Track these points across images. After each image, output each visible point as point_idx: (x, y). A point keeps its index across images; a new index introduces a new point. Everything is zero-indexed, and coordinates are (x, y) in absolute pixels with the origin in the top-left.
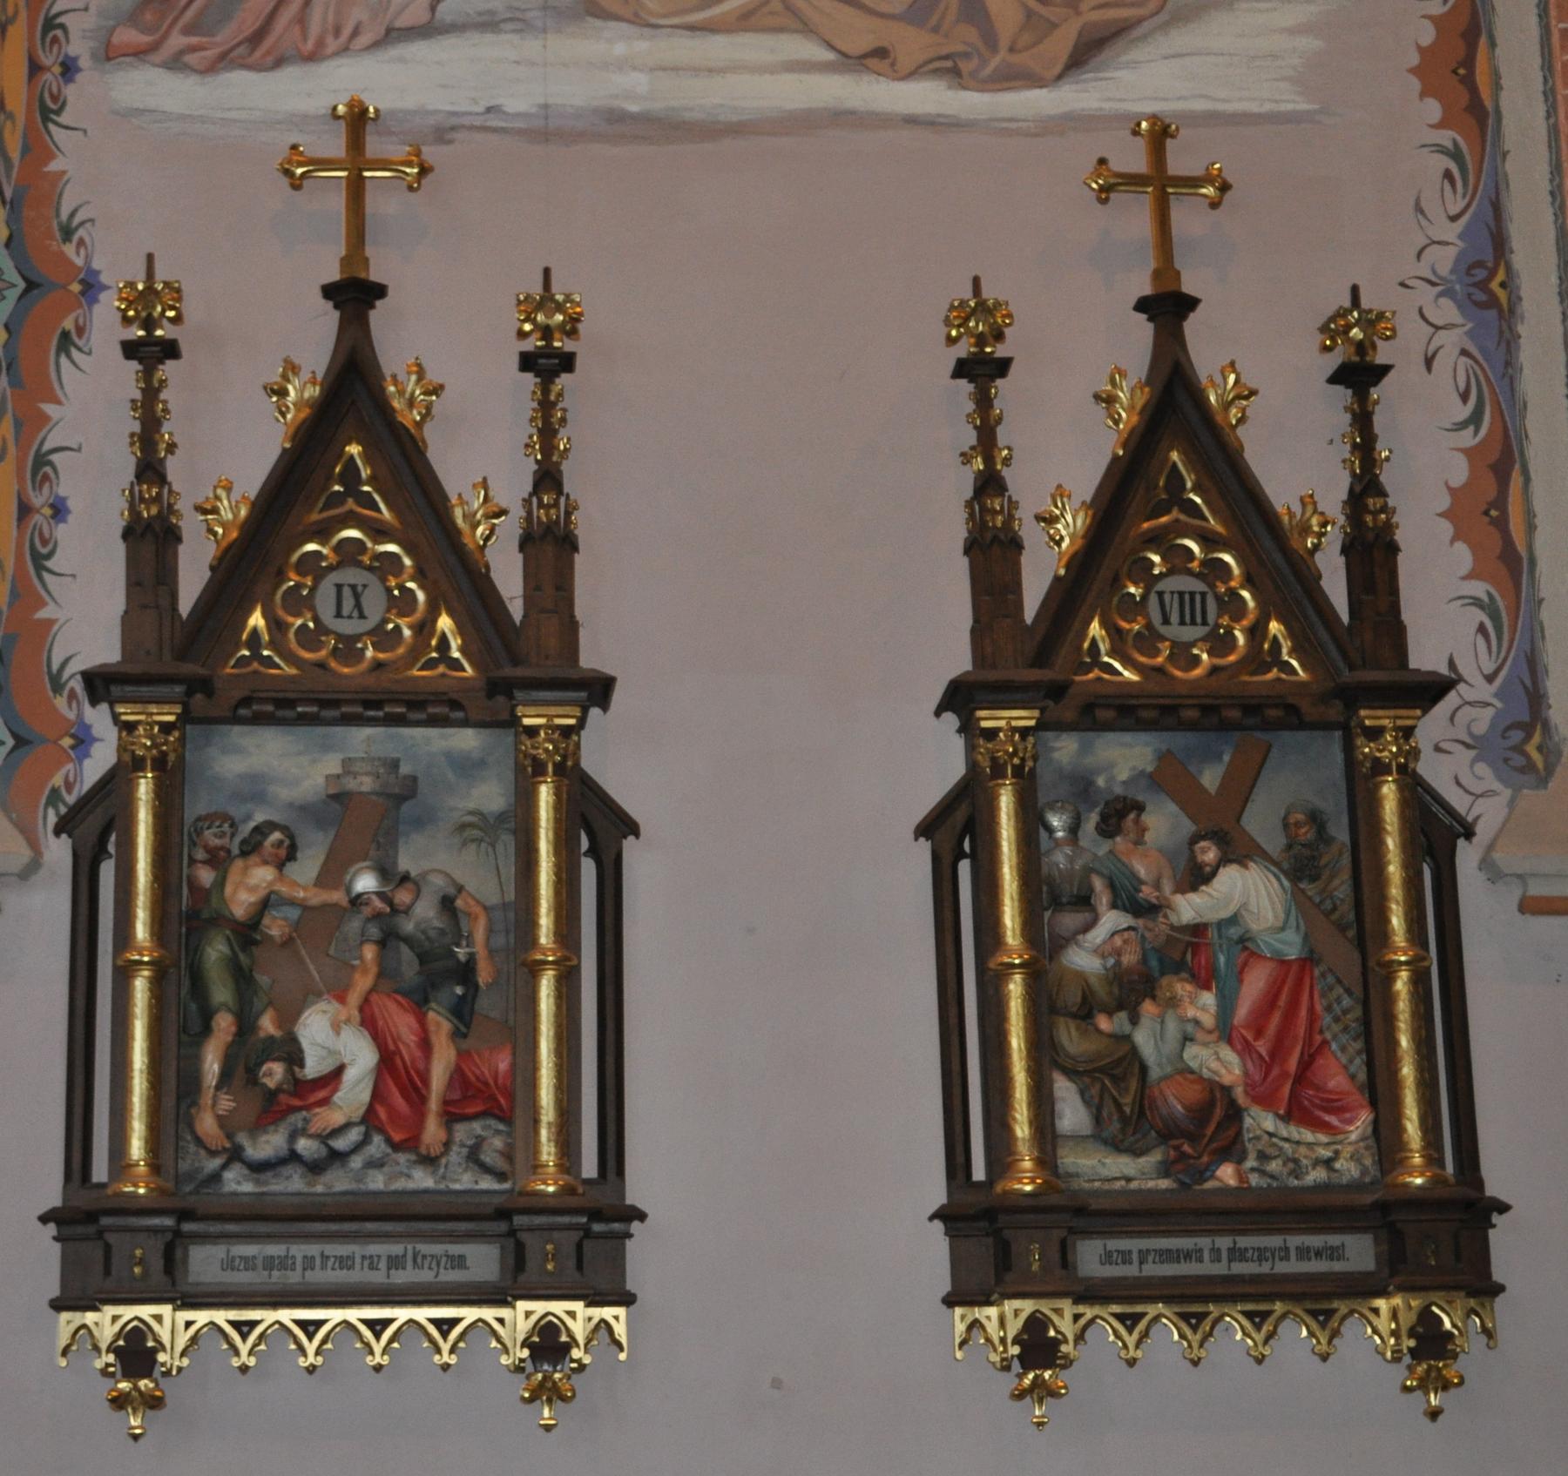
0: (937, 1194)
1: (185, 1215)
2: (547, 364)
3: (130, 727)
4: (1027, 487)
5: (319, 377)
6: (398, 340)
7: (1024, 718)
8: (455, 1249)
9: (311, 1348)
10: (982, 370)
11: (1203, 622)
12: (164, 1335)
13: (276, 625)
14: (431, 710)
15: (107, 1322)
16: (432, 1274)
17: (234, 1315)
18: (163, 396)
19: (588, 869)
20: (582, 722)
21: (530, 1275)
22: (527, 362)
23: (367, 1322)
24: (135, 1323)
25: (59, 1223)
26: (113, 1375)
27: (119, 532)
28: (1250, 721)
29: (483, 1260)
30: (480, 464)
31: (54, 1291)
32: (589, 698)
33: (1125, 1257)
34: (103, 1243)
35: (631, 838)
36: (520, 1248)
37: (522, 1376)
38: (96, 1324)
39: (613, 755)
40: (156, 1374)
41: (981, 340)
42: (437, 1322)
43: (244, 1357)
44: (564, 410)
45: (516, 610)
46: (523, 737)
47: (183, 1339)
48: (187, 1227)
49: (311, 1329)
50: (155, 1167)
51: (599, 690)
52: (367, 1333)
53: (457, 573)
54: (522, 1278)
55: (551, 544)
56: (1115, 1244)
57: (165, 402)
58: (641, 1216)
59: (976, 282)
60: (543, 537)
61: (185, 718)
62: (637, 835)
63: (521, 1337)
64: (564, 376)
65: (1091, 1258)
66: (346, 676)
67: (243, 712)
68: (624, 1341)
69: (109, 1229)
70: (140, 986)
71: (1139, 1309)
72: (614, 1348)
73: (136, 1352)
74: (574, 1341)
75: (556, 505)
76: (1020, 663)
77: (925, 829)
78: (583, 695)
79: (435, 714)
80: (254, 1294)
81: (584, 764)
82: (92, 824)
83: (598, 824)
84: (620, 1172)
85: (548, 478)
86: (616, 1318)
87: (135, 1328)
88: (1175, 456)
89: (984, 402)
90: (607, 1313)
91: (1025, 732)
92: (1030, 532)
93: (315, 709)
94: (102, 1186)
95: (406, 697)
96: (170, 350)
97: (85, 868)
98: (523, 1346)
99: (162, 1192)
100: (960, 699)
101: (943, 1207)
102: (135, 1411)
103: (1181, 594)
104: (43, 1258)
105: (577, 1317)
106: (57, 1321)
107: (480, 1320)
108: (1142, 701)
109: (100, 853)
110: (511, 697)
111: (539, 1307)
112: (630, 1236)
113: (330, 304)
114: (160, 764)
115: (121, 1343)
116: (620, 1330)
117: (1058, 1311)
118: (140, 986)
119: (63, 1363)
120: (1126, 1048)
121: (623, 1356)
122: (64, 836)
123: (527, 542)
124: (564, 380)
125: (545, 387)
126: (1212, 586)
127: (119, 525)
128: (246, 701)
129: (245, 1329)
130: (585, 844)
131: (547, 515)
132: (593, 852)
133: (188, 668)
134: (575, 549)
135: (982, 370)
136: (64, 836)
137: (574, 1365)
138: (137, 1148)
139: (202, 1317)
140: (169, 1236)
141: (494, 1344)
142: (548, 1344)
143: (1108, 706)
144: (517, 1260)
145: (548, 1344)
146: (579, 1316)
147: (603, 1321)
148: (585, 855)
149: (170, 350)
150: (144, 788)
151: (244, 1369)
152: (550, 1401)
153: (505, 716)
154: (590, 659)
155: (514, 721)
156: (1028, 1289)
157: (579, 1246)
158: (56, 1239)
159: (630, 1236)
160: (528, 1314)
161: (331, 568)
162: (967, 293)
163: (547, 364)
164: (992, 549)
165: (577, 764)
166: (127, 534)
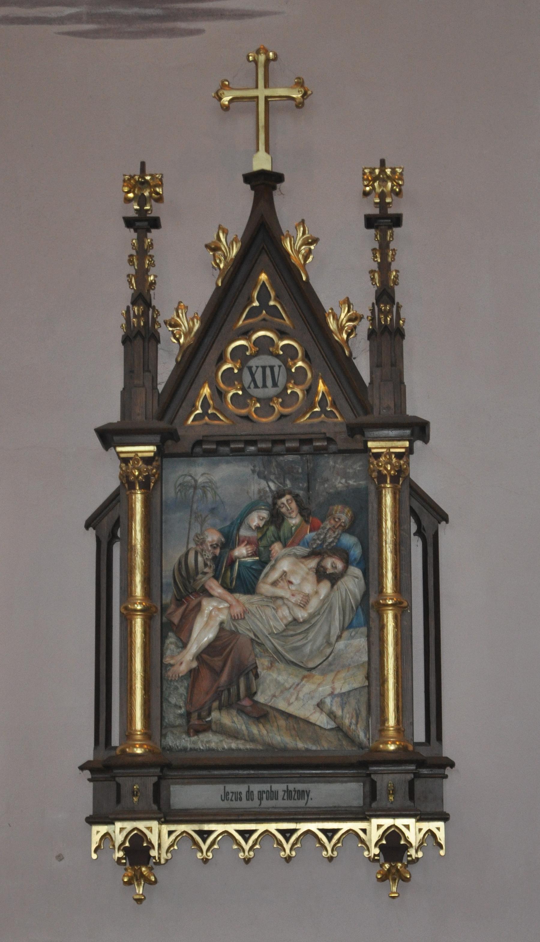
0: (87, 752)
1: (169, 766)
2: (383, 222)
3: (126, 461)
4: (163, 302)
5: (239, 238)
6: (287, 208)
7: (149, 450)
8: (300, 786)
9: (287, 847)
10: (143, 223)
11: (266, 377)
12: (154, 838)
13: (219, 394)
14: (232, 446)
15: (120, 831)
16: (305, 801)
17: (197, 827)
18: (151, 253)
19: (416, 547)
20: (410, 450)
21: (383, 801)
22: (370, 222)
23: (240, 832)
24: (135, 832)
25: (92, 771)
26: (378, 861)
27: (120, 339)
28: (224, 449)
29: (350, 792)
30: (342, 288)
31: (89, 811)
32: (412, 434)
33: (238, 796)
34: (120, 780)
35: (443, 523)
36: (373, 784)
37: (378, 864)
38: (364, 831)
39: (428, 472)
40: (151, 864)
41: (142, 200)
42: (241, 833)
43: (288, 851)
44: (394, 250)
45: (366, 377)
46: (372, 459)
47: (167, 841)
48: (425, 771)
49: (288, 835)
50: (148, 734)
51: (420, 430)
52: (279, 836)
53: (333, 357)
54: (374, 805)
55: (388, 336)
56: (232, 788)
57: (151, 257)
58: (452, 764)
59: (143, 164)
60: (382, 333)
61: (160, 453)
62: (447, 521)
63: (375, 839)
64: (153, 231)
65: (184, 795)
66: (266, 424)
67: (198, 450)
68: (443, 842)
69: (376, 773)
70: (138, 624)
71: (207, 827)
72: (439, 848)
73: (138, 851)
74: (409, 845)
75: (390, 312)
76: (156, 418)
77: (88, 526)
78: (408, 432)
79: (317, 446)
80: (271, 814)
81: (411, 477)
82: (107, 522)
83: (424, 515)
84: (439, 738)
85: (385, 295)
86: (438, 829)
87: (394, 831)
88: (263, 277)
89: (384, 248)
90: (433, 825)
91: (147, 461)
92: (164, 331)
93: (214, 447)
94: (116, 748)
95: (243, 438)
96: (155, 223)
97: (104, 546)
98: (119, 849)
99: (151, 751)
100: (108, 436)
101: (89, 762)
102: (139, 885)
103: (264, 368)
104: (82, 793)
105: (413, 830)
106: (90, 831)
107: (350, 830)
108: (317, 436)
109: (113, 538)
110: (363, 435)
111: (387, 822)
112: (446, 777)
113: (248, 186)
114: (145, 486)
115: (384, 842)
116: (441, 836)
117: (407, 827)
118: (138, 624)
119: (94, 856)
120: (205, 656)
121: (442, 853)
122: (91, 529)
123: (371, 334)
124: (154, 234)
125: (141, 240)
126: (285, 363)
127: (120, 333)
128: (199, 443)
129: (330, 834)
130: (414, 528)
131: (139, 323)
132: (420, 533)
133: (163, 425)
134: (403, 336)
135: (143, 223)
136: (91, 529)
137: (409, 859)
138: (138, 725)
139: (181, 828)
140: (410, 776)
141: (235, 847)
142: (393, 846)
143: (294, 440)
144: (372, 793)
145: (393, 846)
146: (411, 827)
147: (429, 831)
148: (415, 534)
149: (397, 221)
150: (138, 498)
151: (205, 861)
152: (394, 880)
153: (360, 446)
154: (415, 408)
155: (367, 450)
156: (125, 816)
157: (411, 784)
158: (89, 780)
159: (446, 777)
160: (379, 826)
161: (252, 356)
162: (137, 171)
163: (383, 222)
164: (140, 338)
165: (409, 475)
166: (126, 340)
